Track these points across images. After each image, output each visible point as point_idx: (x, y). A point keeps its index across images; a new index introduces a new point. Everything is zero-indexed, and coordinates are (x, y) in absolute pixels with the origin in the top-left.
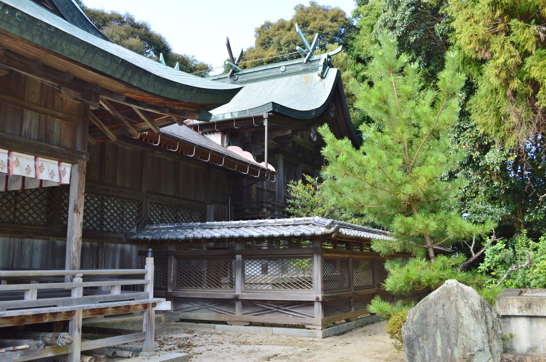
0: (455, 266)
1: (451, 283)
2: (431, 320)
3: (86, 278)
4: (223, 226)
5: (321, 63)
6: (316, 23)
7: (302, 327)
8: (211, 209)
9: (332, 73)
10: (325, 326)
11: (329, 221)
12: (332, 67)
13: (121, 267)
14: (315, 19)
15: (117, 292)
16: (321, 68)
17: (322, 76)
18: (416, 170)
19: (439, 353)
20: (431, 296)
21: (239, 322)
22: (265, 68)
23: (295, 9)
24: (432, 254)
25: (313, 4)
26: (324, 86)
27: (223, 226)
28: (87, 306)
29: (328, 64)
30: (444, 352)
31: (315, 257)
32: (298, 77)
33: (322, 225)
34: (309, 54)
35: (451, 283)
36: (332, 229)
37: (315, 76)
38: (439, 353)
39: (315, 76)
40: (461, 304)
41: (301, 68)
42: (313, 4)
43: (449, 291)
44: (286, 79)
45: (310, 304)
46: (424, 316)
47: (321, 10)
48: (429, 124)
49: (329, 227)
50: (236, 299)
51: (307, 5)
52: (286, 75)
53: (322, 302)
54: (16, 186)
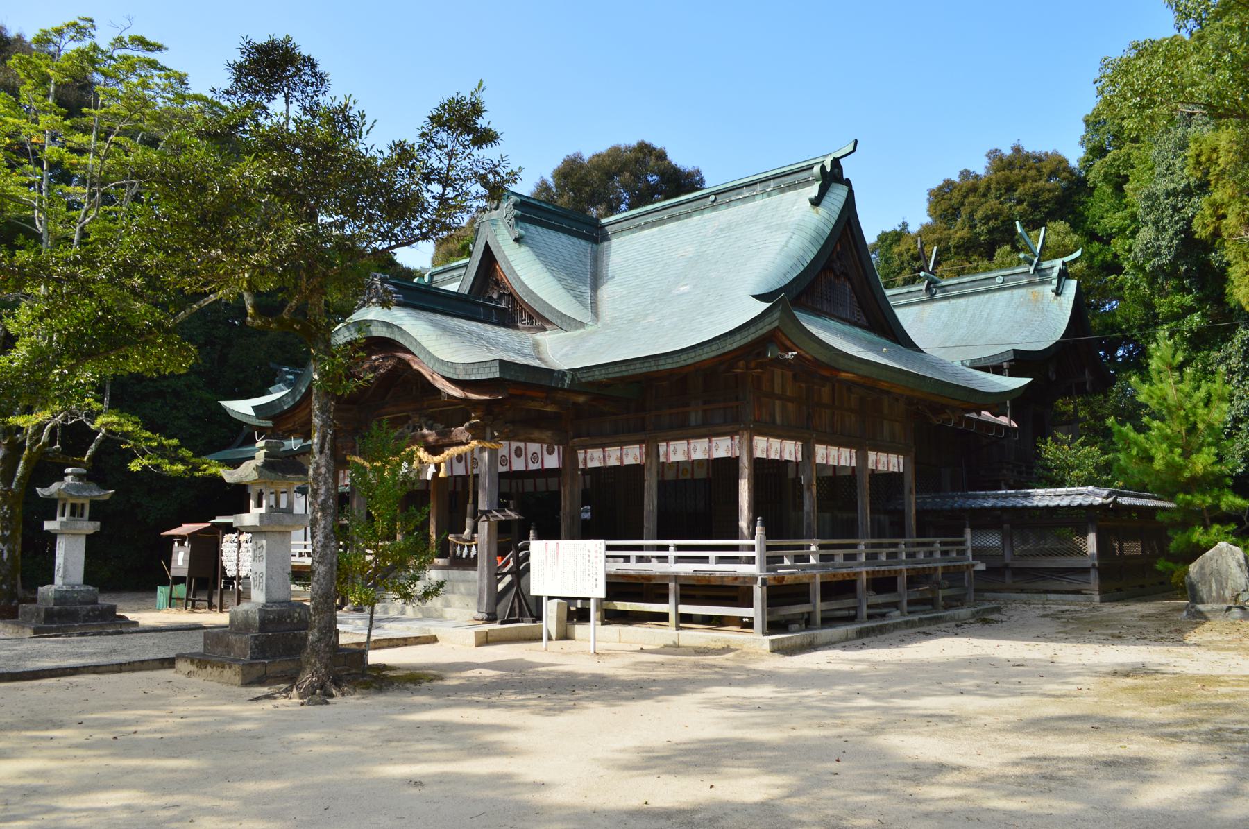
0: (1228, 533)
1: (1222, 544)
2: (1207, 571)
3: (942, 544)
4: (989, 496)
5: (1055, 274)
6: (1028, 185)
7: (1078, 592)
8: (694, 418)
9: (1071, 286)
10: (1103, 592)
11: (1106, 492)
12: (1068, 278)
13: (918, 536)
14: (1024, 180)
15: (954, 555)
16: (1055, 282)
17: (1058, 293)
18: (1194, 456)
19: (1214, 594)
20: (1208, 553)
21: (1009, 590)
22: (973, 278)
23: (988, 155)
24: (1208, 521)
25: (1017, 150)
26: (1060, 305)
27: (989, 496)
28: (869, 569)
29: (1064, 274)
30: (1218, 593)
31: (98, 523)
32: (1022, 291)
33: (1098, 495)
34: (1036, 260)
35: (1222, 544)
36: (1110, 500)
37: (1048, 290)
38: (1214, 594)
39: (1048, 290)
40: (1230, 559)
41: (1026, 280)
42: (1017, 150)
43: (1221, 550)
44: (1006, 294)
45: (1085, 571)
46: (1202, 568)
47: (1031, 161)
48: (1203, 421)
49: (1107, 497)
50: (1006, 567)
51: (1007, 151)
52: (1005, 289)
53: (1099, 569)
54: (830, 473)
